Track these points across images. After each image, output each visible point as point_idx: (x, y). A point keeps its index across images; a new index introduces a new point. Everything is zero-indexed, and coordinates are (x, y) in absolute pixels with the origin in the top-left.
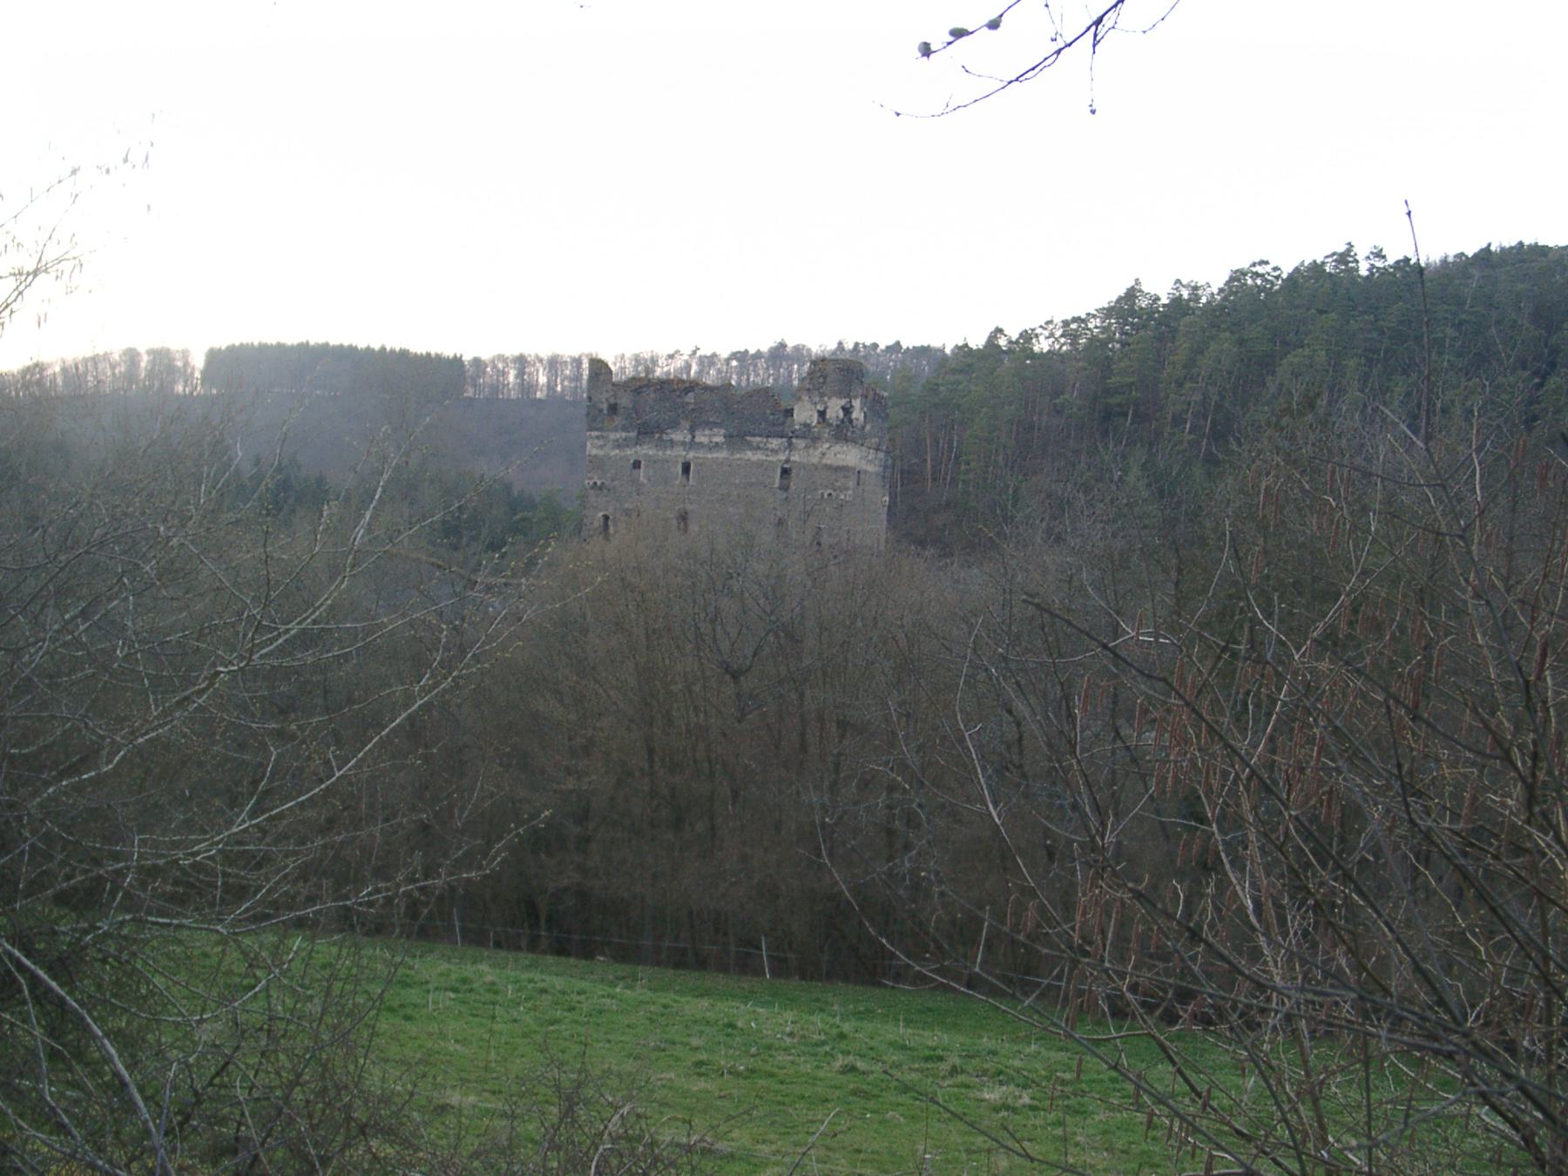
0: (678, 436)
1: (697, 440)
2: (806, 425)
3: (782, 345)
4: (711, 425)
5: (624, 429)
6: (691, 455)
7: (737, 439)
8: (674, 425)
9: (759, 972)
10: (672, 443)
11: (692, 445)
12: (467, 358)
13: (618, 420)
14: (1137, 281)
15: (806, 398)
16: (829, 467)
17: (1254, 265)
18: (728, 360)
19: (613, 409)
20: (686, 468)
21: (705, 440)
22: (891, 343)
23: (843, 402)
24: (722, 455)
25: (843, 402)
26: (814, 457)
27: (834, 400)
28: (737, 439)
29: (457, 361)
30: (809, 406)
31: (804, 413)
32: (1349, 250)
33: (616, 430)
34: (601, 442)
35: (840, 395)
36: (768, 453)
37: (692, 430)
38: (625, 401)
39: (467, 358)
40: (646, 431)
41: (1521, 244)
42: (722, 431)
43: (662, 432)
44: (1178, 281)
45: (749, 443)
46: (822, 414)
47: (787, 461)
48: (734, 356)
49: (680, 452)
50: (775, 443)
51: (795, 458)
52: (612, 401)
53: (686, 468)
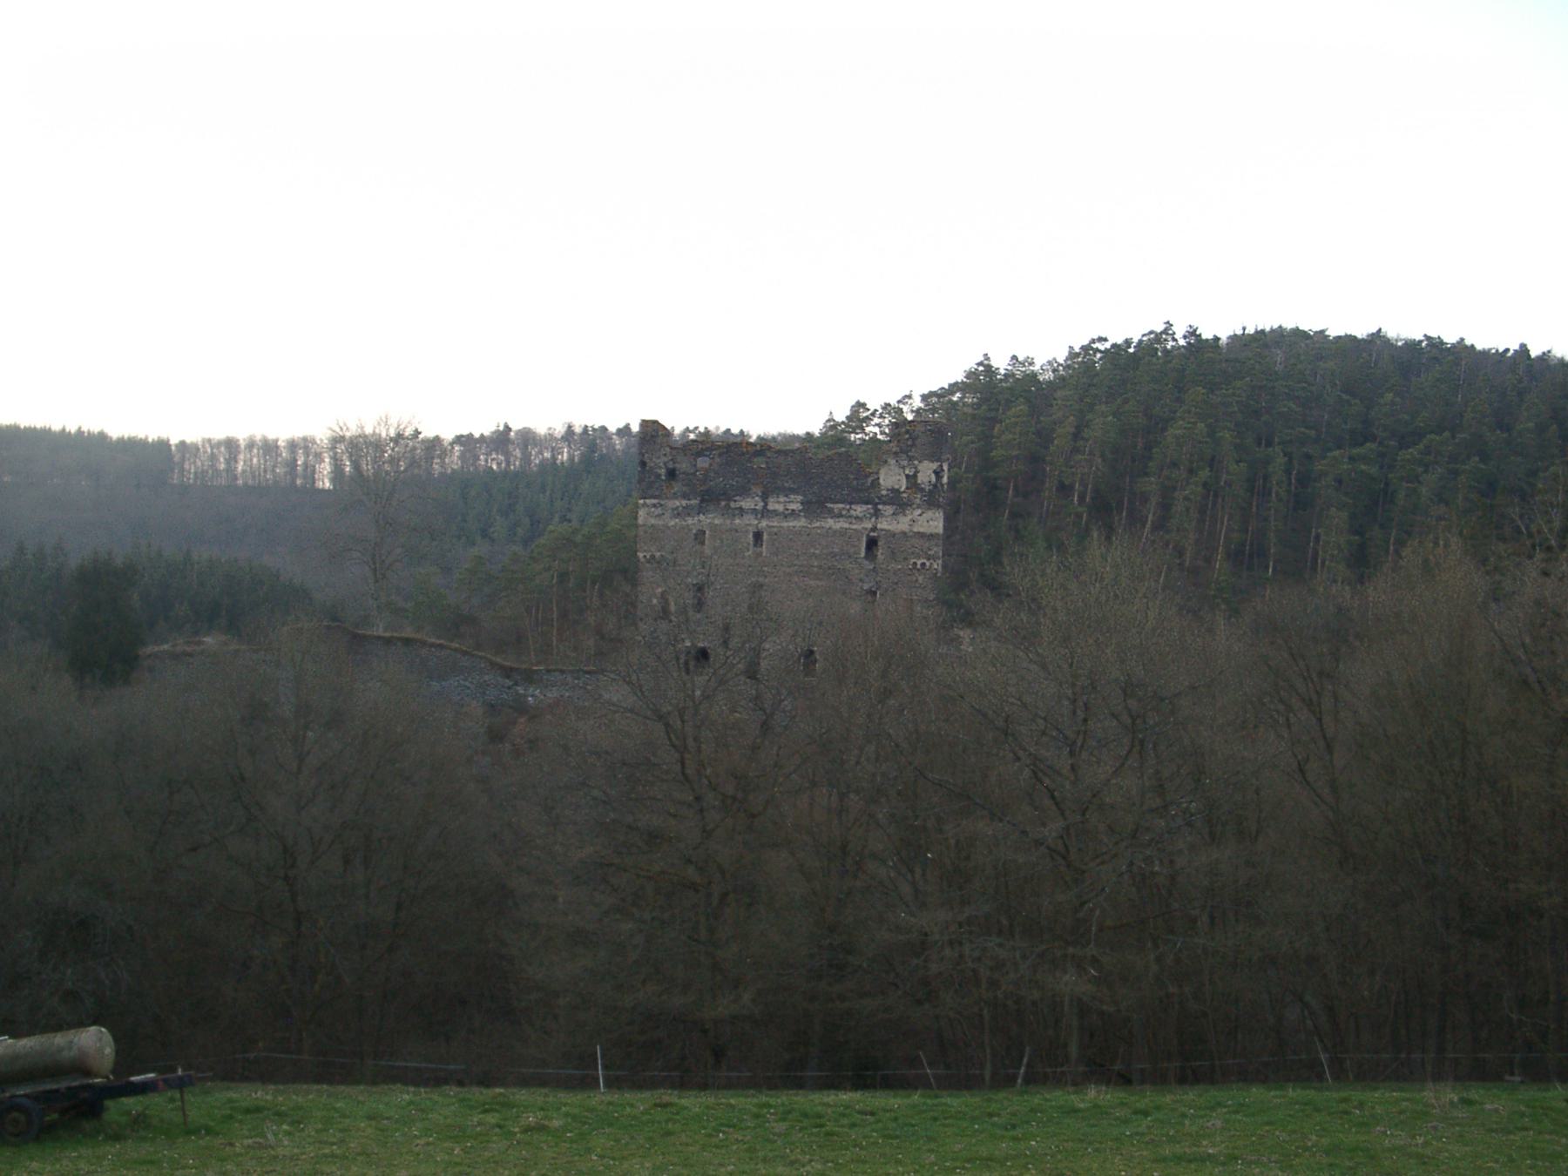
0: (747, 504)
1: (770, 507)
2: (893, 490)
3: (508, 429)
4: (788, 492)
5: (685, 496)
6: (764, 523)
7: (815, 507)
8: (744, 491)
9: (1320, 1077)
10: (741, 511)
11: (765, 513)
12: (174, 441)
13: (677, 487)
14: (986, 357)
15: (892, 462)
16: (922, 535)
17: (1093, 341)
18: (452, 444)
19: (672, 474)
20: (758, 536)
21: (780, 508)
22: (621, 426)
23: (935, 466)
24: (802, 522)
25: (935, 466)
26: (902, 524)
27: (926, 463)
28: (815, 507)
29: (163, 445)
30: (897, 470)
31: (891, 477)
32: (1165, 332)
33: (675, 496)
34: (659, 511)
35: (933, 457)
36: (852, 521)
37: (765, 497)
38: (683, 465)
39: (174, 441)
40: (710, 498)
41: (1523, 347)
42: (800, 498)
43: (729, 499)
44: (1014, 358)
45: (831, 511)
46: (912, 479)
47: (874, 529)
48: (459, 439)
49: (751, 520)
50: (859, 510)
51: (883, 525)
52: (671, 465)
53: (758, 536)
